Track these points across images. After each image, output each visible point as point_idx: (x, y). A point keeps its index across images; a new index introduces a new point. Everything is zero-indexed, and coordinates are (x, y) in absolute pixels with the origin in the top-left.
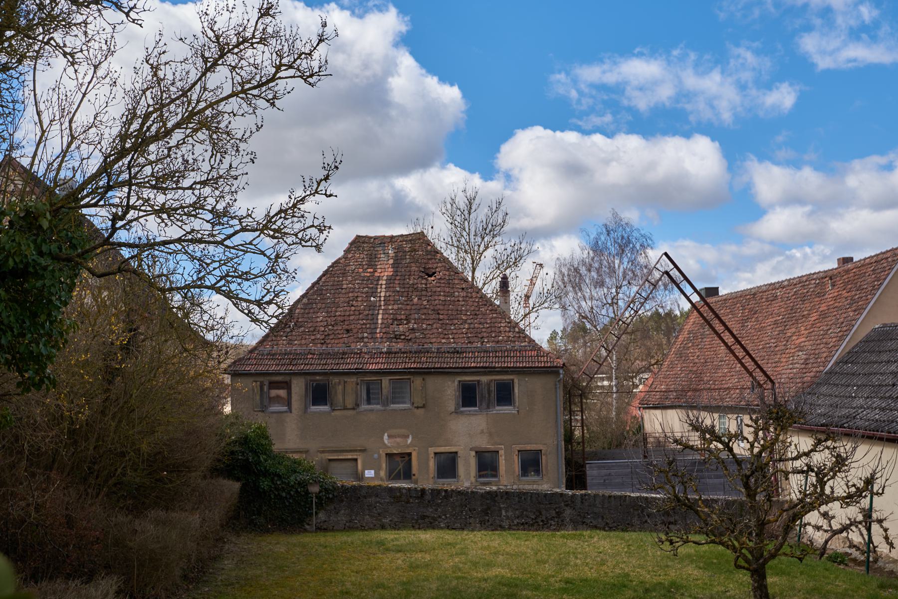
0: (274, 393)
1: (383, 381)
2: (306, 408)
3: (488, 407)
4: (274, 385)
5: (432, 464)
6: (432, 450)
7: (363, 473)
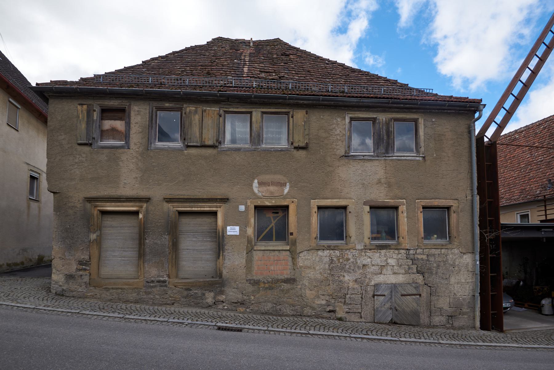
0: (108, 124)
1: (254, 114)
2: (149, 142)
3: (387, 151)
4: (107, 113)
5: (315, 220)
6: (315, 203)
7: (224, 230)
